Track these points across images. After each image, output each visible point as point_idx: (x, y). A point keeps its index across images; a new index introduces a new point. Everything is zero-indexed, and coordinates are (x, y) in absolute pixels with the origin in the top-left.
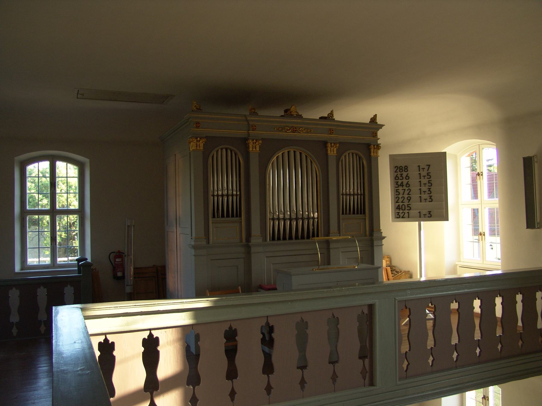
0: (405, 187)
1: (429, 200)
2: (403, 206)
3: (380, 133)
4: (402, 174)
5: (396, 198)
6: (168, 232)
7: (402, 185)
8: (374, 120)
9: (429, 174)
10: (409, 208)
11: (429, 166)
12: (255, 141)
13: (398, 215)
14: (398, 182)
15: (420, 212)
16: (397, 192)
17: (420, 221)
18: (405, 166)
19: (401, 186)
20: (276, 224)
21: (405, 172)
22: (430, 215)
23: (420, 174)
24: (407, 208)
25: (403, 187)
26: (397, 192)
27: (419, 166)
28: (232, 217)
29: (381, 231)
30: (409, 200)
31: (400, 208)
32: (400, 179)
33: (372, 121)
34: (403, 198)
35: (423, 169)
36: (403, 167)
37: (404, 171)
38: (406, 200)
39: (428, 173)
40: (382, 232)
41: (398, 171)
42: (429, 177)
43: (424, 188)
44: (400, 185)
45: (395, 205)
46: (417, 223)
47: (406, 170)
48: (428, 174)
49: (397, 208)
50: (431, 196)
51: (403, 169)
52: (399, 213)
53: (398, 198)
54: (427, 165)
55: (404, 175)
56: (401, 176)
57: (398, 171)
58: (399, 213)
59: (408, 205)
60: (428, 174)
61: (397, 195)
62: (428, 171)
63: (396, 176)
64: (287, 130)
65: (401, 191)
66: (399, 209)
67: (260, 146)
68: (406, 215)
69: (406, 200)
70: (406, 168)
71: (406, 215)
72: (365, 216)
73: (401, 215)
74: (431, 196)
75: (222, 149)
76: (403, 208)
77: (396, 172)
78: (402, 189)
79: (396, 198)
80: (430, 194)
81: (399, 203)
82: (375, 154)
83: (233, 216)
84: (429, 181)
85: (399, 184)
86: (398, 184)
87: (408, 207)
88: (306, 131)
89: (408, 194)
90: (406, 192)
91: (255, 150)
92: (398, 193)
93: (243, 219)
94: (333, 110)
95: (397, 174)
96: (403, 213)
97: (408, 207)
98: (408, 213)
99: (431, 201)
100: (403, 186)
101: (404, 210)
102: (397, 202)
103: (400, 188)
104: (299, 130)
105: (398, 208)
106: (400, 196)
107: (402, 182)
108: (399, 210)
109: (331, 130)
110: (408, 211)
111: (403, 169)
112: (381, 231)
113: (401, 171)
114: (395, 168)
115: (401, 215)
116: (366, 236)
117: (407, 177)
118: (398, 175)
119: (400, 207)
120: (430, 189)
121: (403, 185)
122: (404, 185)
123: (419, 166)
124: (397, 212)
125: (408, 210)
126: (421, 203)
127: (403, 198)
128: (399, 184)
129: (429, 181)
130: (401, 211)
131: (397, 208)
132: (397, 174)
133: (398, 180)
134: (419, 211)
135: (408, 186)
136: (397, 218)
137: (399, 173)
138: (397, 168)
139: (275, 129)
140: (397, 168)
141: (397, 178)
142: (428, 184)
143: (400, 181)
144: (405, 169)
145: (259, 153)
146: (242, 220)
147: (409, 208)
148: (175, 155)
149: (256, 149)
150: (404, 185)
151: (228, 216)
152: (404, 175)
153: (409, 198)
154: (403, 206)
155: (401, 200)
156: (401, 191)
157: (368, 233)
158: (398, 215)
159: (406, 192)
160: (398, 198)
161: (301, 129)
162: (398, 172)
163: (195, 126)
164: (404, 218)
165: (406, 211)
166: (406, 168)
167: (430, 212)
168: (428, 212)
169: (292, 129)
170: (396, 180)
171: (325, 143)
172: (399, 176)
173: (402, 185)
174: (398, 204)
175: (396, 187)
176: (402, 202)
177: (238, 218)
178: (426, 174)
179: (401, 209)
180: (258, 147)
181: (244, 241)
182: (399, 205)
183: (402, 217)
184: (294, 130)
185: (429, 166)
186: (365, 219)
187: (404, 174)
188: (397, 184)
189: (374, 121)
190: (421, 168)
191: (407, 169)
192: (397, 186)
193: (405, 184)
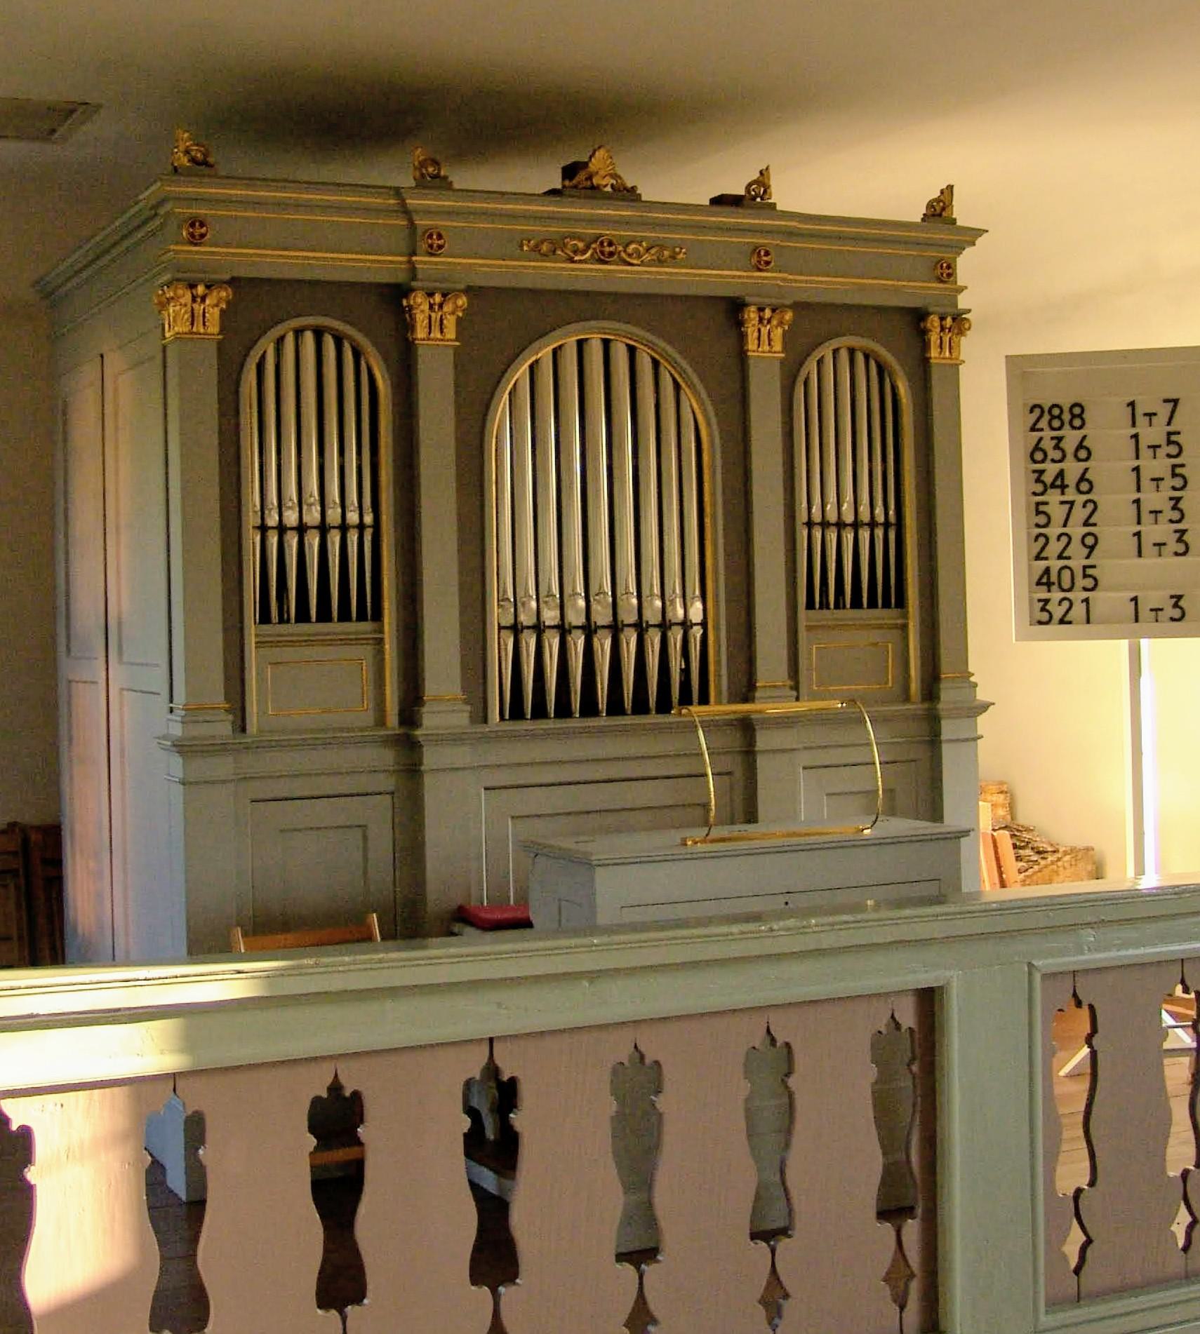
0: (1075, 491)
1: (1173, 546)
2: (1066, 575)
3: (966, 264)
4: (1060, 439)
5: (1036, 539)
6: (70, 682)
7: (1058, 483)
8: (939, 210)
9: (1173, 438)
10: (1089, 583)
11: (1175, 402)
12: (438, 298)
13: (1043, 609)
14: (1041, 472)
15: (1135, 599)
16: (1038, 513)
17: (1134, 637)
18: (1076, 405)
19: (1057, 487)
20: (527, 650)
21: (1074, 428)
22: (1177, 613)
23: (1136, 436)
24: (1080, 582)
25: (1066, 490)
26: (1038, 513)
27: (1132, 404)
28: (298, 620)
29: (972, 679)
30: (1092, 548)
31: (1054, 584)
32: (1053, 461)
33: (933, 215)
34: (1064, 540)
35: (1150, 415)
36: (1066, 409)
37: (1067, 426)
38: (1076, 550)
39: (1169, 434)
40: (975, 685)
41: (1043, 423)
42: (1173, 450)
43: (1154, 499)
44: (1053, 486)
45: (1030, 567)
46: (1124, 643)
47: (1077, 422)
48: (1171, 439)
49: (1039, 583)
50: (1183, 532)
51: (1066, 417)
52: (1046, 601)
53: (1042, 540)
54: (1166, 401)
55: (1070, 444)
56: (1057, 447)
57: (1043, 423)
58: (1046, 601)
59: (1085, 567)
60: (1171, 439)
61: (1038, 526)
62: (1169, 424)
63: (1037, 448)
64: (575, 252)
65: (1058, 512)
66: (1049, 585)
67: (459, 321)
68: (1078, 611)
69: (1076, 550)
70: (1078, 414)
71: (1078, 611)
72: (905, 616)
73: (1058, 612)
74: (1183, 532)
75: (298, 333)
76: (1066, 584)
77: (1033, 429)
78: (1062, 503)
79: (1036, 539)
80: (1179, 521)
81: (1046, 559)
82: (947, 354)
83: (345, 616)
84: (1174, 466)
85: (1048, 478)
86: (1043, 482)
87: (1085, 576)
88: (655, 257)
89: (1086, 523)
90: (1080, 514)
91: (439, 336)
92: (1042, 520)
93: (386, 628)
94: (767, 169)
95: (1041, 439)
96: (1066, 604)
97: (1085, 576)
98: (1086, 601)
99: (1184, 554)
100: (1063, 487)
101: (1070, 590)
102: (1038, 558)
103: (1054, 497)
104: (625, 251)
105: (1044, 580)
106: (1053, 531)
107: (1061, 474)
108: (1049, 591)
109: (762, 253)
110: (1085, 595)
111: (1066, 417)
112: (972, 679)
113: (1056, 423)
114: (1031, 411)
115: (1058, 612)
116: (907, 698)
117: (1083, 451)
118: (1042, 442)
119: (1054, 578)
120: (1178, 500)
121: (1066, 482)
122: (1067, 486)
123: (1132, 404)
124: (1040, 600)
125: (1085, 589)
126: (1141, 560)
127: (1064, 540)
128: (1048, 478)
129: (1174, 466)
130: (1056, 595)
131: (1039, 583)
132: (1041, 439)
133: (1043, 461)
134: (1133, 595)
135: (1084, 486)
136: (1040, 623)
137: (1048, 434)
138: (1037, 412)
139: (525, 248)
140: (1037, 412)
141: (1039, 456)
142: (1169, 482)
143: (1051, 470)
144: (1073, 416)
145: (456, 348)
146: (381, 631)
147: (1089, 583)
148: (102, 356)
149: (442, 332)
150: (1067, 486)
151: (324, 616)
152: (1070, 444)
153: (1090, 541)
154: (1066, 575)
155: (1054, 548)
156: (1058, 512)
157: (915, 686)
158: (1043, 609)
159: (1080, 514)
160: (1042, 540)
161: (633, 246)
162: (1042, 430)
163: (184, 233)
164: (1070, 623)
165: (1077, 596)
166: (1078, 414)
167: (1179, 597)
168: (1172, 597)
169: (593, 246)
170: (1035, 462)
171: (735, 307)
172: (1048, 445)
173: (1059, 483)
174: (1042, 564)
175: (1035, 494)
176: (1060, 557)
177: (366, 626)
178: (1162, 440)
179: (1055, 588)
180: (450, 323)
181: (392, 718)
182: (1047, 571)
183: (1062, 622)
184: (602, 252)
185: (1175, 402)
186: (904, 628)
187: (1071, 439)
188: (1038, 480)
189: (940, 215)
190: (1140, 411)
191: (1080, 416)
192: (1039, 488)
193: (1071, 479)
